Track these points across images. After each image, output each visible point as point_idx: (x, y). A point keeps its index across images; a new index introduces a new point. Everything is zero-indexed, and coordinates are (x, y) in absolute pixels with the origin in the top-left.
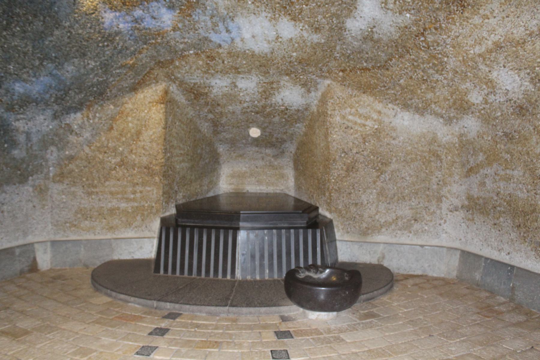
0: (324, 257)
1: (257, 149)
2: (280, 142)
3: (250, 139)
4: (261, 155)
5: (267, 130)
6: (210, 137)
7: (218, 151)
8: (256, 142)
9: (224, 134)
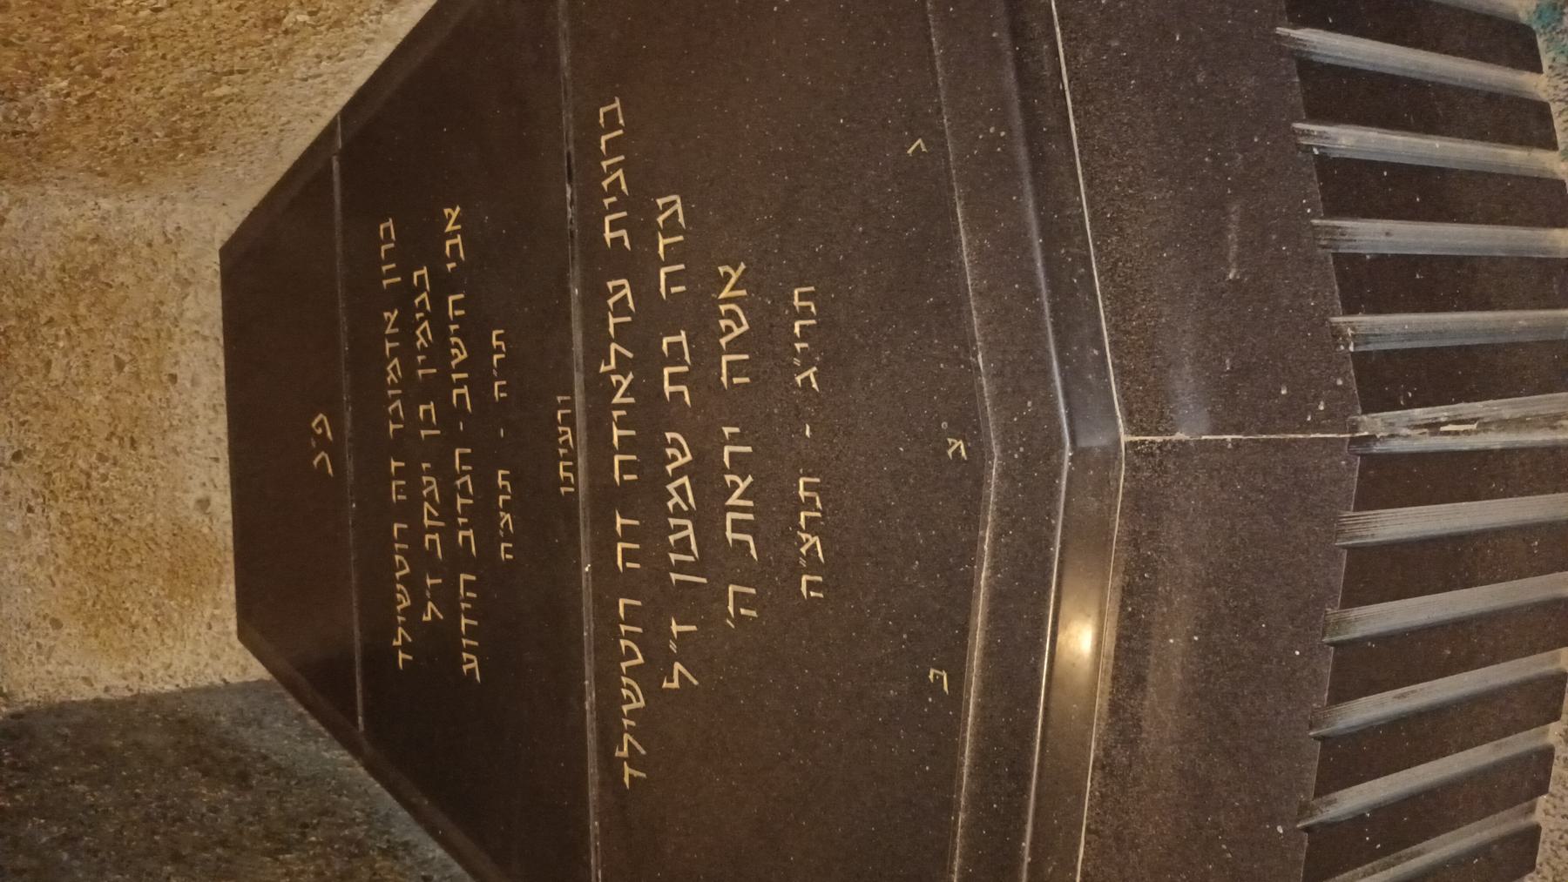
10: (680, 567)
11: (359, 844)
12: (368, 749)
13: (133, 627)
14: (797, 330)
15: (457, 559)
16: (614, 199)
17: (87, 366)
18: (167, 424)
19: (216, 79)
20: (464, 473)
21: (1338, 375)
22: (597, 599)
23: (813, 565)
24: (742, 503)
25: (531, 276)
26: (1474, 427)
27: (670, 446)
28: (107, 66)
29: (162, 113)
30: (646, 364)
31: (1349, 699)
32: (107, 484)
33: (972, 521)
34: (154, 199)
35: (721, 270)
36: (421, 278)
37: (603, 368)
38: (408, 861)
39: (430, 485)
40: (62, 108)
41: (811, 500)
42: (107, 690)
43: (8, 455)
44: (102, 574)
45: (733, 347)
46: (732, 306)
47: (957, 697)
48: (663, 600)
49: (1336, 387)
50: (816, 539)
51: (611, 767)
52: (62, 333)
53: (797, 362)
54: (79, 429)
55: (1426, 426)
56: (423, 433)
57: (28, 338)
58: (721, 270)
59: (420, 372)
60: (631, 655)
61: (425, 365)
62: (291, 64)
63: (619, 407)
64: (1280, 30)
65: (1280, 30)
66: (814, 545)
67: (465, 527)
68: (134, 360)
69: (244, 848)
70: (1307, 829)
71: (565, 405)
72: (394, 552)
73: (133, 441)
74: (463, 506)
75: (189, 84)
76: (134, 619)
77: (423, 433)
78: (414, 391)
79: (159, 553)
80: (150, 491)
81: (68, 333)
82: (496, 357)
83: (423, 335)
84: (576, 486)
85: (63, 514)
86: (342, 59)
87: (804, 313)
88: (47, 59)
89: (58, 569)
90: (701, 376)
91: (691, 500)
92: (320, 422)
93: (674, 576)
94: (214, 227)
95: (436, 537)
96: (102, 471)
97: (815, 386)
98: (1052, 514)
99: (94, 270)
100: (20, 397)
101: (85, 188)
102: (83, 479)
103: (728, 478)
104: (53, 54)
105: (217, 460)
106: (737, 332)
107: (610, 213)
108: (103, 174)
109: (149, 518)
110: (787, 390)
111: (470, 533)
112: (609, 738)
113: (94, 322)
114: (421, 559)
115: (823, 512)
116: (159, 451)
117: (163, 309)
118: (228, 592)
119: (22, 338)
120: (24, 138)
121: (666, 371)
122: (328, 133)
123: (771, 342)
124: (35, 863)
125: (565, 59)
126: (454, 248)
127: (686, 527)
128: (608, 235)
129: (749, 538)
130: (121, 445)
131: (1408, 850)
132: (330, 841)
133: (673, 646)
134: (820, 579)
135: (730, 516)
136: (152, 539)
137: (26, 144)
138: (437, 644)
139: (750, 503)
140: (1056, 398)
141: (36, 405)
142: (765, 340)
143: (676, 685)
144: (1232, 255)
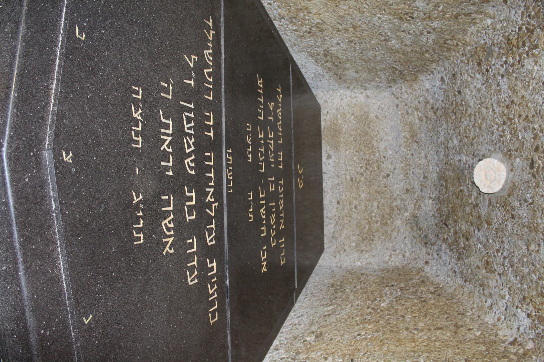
2: (456, 241)
6: (465, 44)
7: (422, 77)
10: (190, 110)
11: (291, 22)
13: (353, 114)
14: (142, 222)
16: (213, 281)
17: (366, 207)
18: (341, 186)
19: (334, 312)
20: (261, 161)
22: (220, 102)
23: (136, 102)
24: (165, 138)
27: (193, 167)
28: (370, 313)
29: (348, 298)
30: (201, 207)
32: (361, 165)
33: (60, 116)
34: (343, 266)
35: (173, 251)
37: (217, 204)
40: (381, 296)
41: (136, 136)
42: (362, 93)
43: (391, 177)
44: (363, 134)
45: (168, 213)
46: (168, 233)
50: (135, 116)
51: (216, 27)
52: (373, 218)
53: (142, 206)
54: (369, 185)
56: (273, 179)
57: (384, 216)
58: (173, 251)
59: (274, 204)
62: (309, 321)
63: (211, 187)
66: (136, 113)
67: (261, 139)
68: (351, 209)
69: (332, 27)
72: (282, 132)
75: (342, 309)
76: (353, 117)
77: (273, 179)
79: (344, 140)
80: (347, 162)
81: (372, 218)
82: (251, 210)
84: (226, 152)
85: (374, 155)
86: (291, 324)
87: (139, 230)
88: (390, 313)
89: (376, 136)
90: (181, 198)
91: (185, 141)
95: (270, 136)
96: (362, 170)
97: (134, 194)
100: (387, 196)
101: (367, 269)
102: (368, 167)
104: (388, 315)
106: (166, 221)
108: (362, 274)
109: (347, 153)
110: (146, 192)
111: (260, 136)
112: (217, 38)
114: (275, 129)
115: (131, 129)
116: (344, 177)
119: (386, 216)
120: (390, 285)
121: (194, 203)
123: (152, 216)
124: (398, 34)
127: (188, 128)
130: (356, 179)
132: (302, 25)
133: (193, 74)
134: (134, 96)
135: (170, 132)
136: (346, 145)
137: (388, 283)
139: (162, 137)
140: (11, 183)
141: (382, 193)
142: (155, 217)
143: (193, 57)
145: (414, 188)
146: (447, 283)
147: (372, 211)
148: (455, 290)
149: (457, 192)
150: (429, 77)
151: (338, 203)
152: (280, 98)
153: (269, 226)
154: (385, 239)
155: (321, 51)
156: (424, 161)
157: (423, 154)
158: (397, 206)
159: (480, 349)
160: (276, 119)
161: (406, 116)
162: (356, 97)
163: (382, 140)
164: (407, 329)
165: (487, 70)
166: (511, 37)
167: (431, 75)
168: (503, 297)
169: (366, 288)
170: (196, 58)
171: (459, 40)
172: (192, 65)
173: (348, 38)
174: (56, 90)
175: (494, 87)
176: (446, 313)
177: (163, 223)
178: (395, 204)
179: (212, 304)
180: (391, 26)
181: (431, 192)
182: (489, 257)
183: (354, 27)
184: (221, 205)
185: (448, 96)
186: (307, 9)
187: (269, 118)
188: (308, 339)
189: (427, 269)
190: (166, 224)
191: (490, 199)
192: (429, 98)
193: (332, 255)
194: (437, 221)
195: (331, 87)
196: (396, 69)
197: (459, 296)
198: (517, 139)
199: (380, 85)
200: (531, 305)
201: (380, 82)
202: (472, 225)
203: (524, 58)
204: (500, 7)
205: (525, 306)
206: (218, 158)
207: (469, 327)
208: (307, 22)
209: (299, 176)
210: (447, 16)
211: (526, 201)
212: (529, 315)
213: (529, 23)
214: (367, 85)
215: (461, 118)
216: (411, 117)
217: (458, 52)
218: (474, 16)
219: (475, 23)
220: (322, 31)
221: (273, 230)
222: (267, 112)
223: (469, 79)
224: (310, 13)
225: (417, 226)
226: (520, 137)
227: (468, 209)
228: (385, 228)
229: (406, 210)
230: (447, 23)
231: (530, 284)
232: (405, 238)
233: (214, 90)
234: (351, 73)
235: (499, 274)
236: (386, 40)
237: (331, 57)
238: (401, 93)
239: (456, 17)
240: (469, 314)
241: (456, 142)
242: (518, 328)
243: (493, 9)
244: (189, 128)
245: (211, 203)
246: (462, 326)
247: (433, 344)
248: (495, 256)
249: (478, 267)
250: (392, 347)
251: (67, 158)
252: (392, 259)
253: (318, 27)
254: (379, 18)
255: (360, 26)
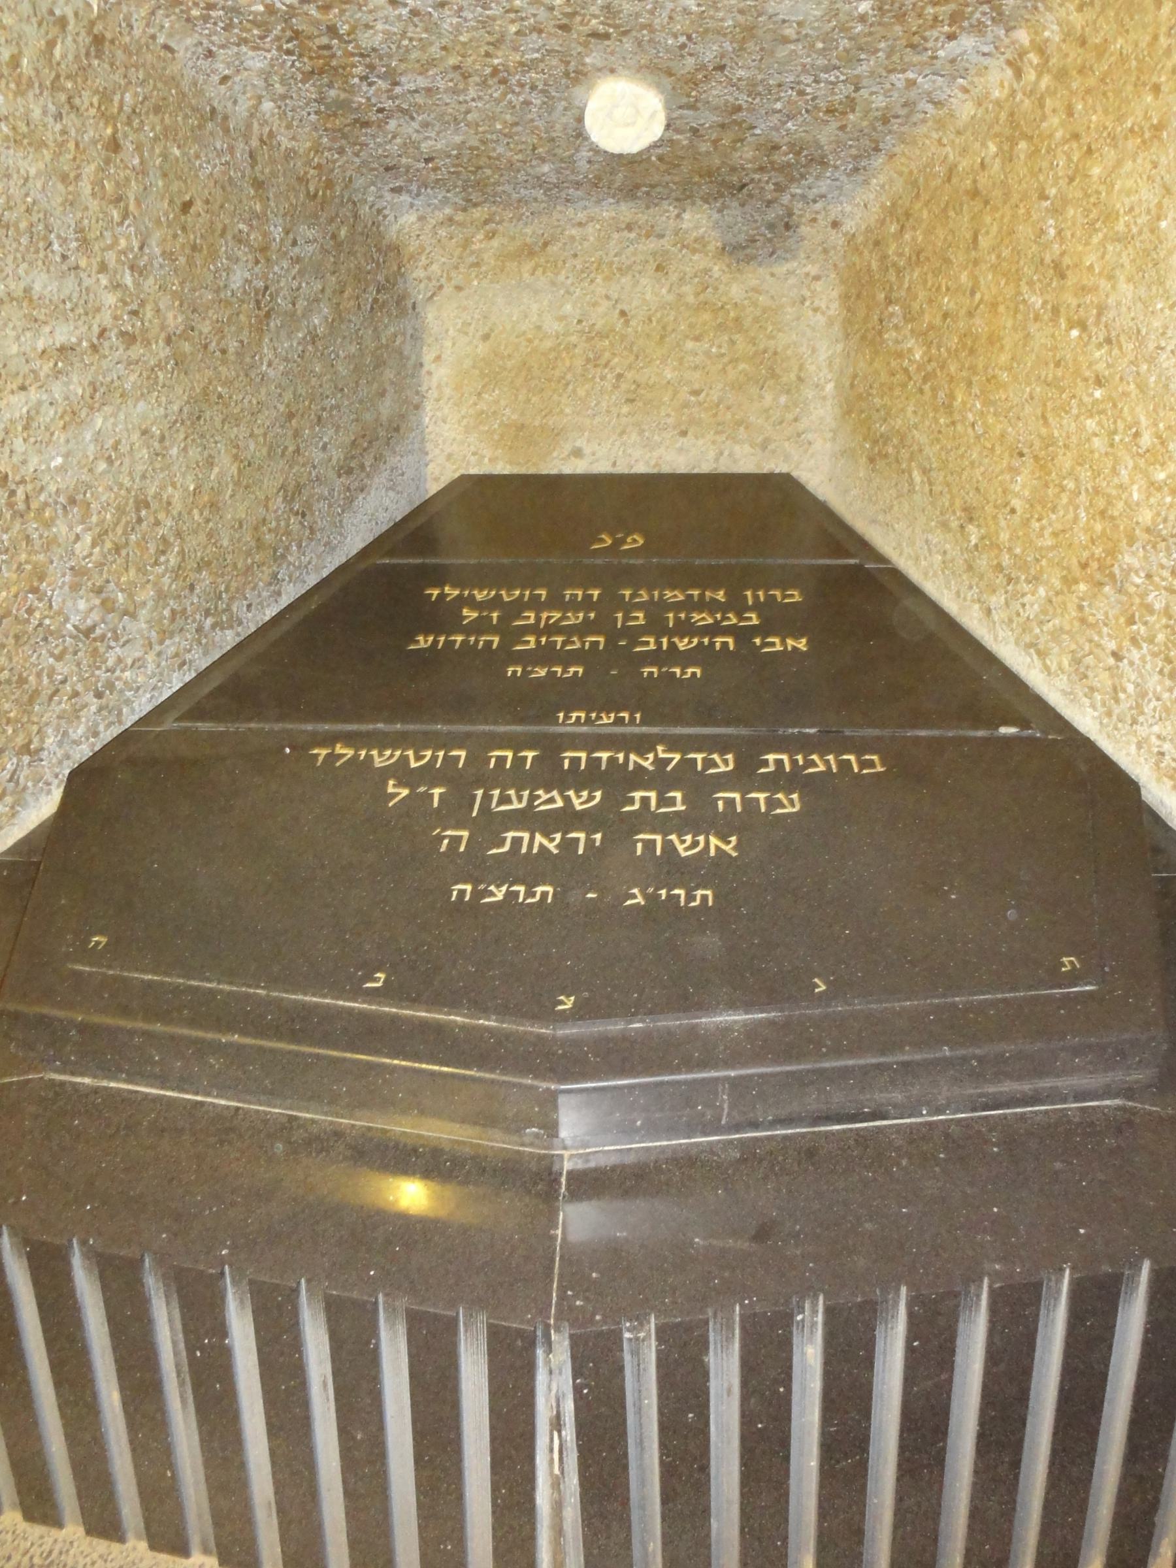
0: (1153, 1506)
1: (626, 211)
2: (784, 168)
3: (585, 154)
4: (652, 244)
5: (717, 92)
6: (317, 149)
7: (392, 233)
8: (629, 177)
9: (410, 129)
10: (487, 797)
11: (283, 556)
12: (362, 566)
15: (512, 635)
17: (696, 368)
19: (925, 472)
21: (604, 1316)
22: (468, 735)
23: (477, 895)
25: (746, 701)
26: (557, 1471)
30: (661, 779)
31: (329, 1320)
33: (503, 1011)
35: (733, 839)
36: (750, 619)
38: (265, 594)
39: (575, 618)
41: (533, 895)
42: (429, 373)
43: (626, 308)
46: (702, 845)
47: (357, 992)
48: (461, 784)
49: (593, 1315)
51: (329, 740)
53: (651, 890)
55: (558, 1413)
59: (671, 615)
60: (418, 758)
61: (677, 619)
63: (627, 759)
64: (904, 1290)
65: (904, 1290)
67: (538, 642)
68: (700, 404)
70: (222, 1274)
71: (632, 719)
72: (523, 588)
73: (632, 401)
74: (600, 759)
77: (620, 615)
78: (655, 611)
81: (723, 355)
83: (702, 619)
84: (563, 723)
87: (690, 898)
89: (530, 341)
90: (645, 819)
92: (637, 540)
93: (480, 793)
94: (811, 470)
95: (532, 621)
98: (504, 1071)
99: (773, 375)
102: (603, 361)
103: (558, 836)
105: (614, 464)
107: (790, 758)
108: (852, 386)
112: (350, 739)
113: (732, 374)
114: (517, 608)
116: (624, 420)
117: (742, 429)
118: (502, 468)
119: (719, 320)
122: (881, 558)
123: (668, 872)
125: (923, 733)
126: (773, 644)
128: (771, 757)
129: (506, 848)
130: (629, 391)
131: (189, 1391)
132: (288, 533)
133: (422, 789)
135: (526, 836)
138: (442, 618)
139: (535, 851)
141: (664, 328)
142: (672, 868)
143: (390, 790)
144: (715, 1242)
145: (654, 254)
146: (882, 187)
147: (707, 354)
148: (901, 174)
149: (663, 167)
150: (391, 218)
151: (684, 433)
152: (452, 592)
153: (714, 630)
154: (773, 324)
155: (339, 483)
156: (590, 230)
157: (574, 232)
158: (697, 294)
159: (1022, 156)
160: (496, 602)
161: (484, 268)
162: (439, 386)
163: (539, 328)
164: (970, 314)
165: (381, 110)
166: (308, 68)
167: (386, 212)
168: (911, 83)
169: (882, 385)
170: (391, 782)
171: (308, 163)
172: (405, 792)
173: (312, 428)
174: (464, 1016)
175: (419, 99)
176: (945, 210)
177: (684, 854)
178: (691, 299)
179: (845, 766)
180: (283, 333)
181: (665, 215)
182: (816, 107)
183: (291, 416)
184: (661, 739)
185: (437, 181)
186: (256, 529)
187: (495, 621)
188: (974, 540)
189: (849, 226)
190: (686, 849)
191: (680, 107)
192: (440, 215)
193: (806, 451)
194: (735, 204)
195: (416, 446)
196: (375, 301)
197: (913, 166)
198: (542, 60)
199: (410, 332)
200: (927, 34)
201: (404, 334)
202: (742, 140)
203: (358, 47)
204: (236, 87)
205: (930, 45)
206: (575, 741)
207: (977, 166)
208: (282, 523)
209: (618, 543)
210: (258, 207)
211: (683, 46)
212: (951, 37)
213: (278, 39)
214: (411, 363)
215: (490, 158)
216: (485, 256)
217: (335, 162)
218: (254, 143)
219: (271, 134)
220: (299, 488)
221: (724, 618)
222: (481, 626)
223: (398, 140)
224: (264, 520)
225: (744, 248)
226: (536, 55)
227: (704, 147)
228: (747, 322)
229: (707, 271)
230: (272, 204)
231: (878, 36)
232: (773, 275)
233: (447, 747)
234: (386, 407)
235: (857, 89)
236: (314, 338)
237: (353, 457)
238: (429, 279)
239: (258, 184)
240: (951, 156)
241: (546, 168)
242: (984, 54)
243: (240, 101)
244: (520, 798)
245: (658, 761)
246: (975, 181)
247: (1005, 264)
248: (814, 99)
249: (842, 128)
250: (1004, 358)
251: (567, 1003)
252: (823, 307)
253: (293, 499)
254: (270, 365)
255: (288, 406)
